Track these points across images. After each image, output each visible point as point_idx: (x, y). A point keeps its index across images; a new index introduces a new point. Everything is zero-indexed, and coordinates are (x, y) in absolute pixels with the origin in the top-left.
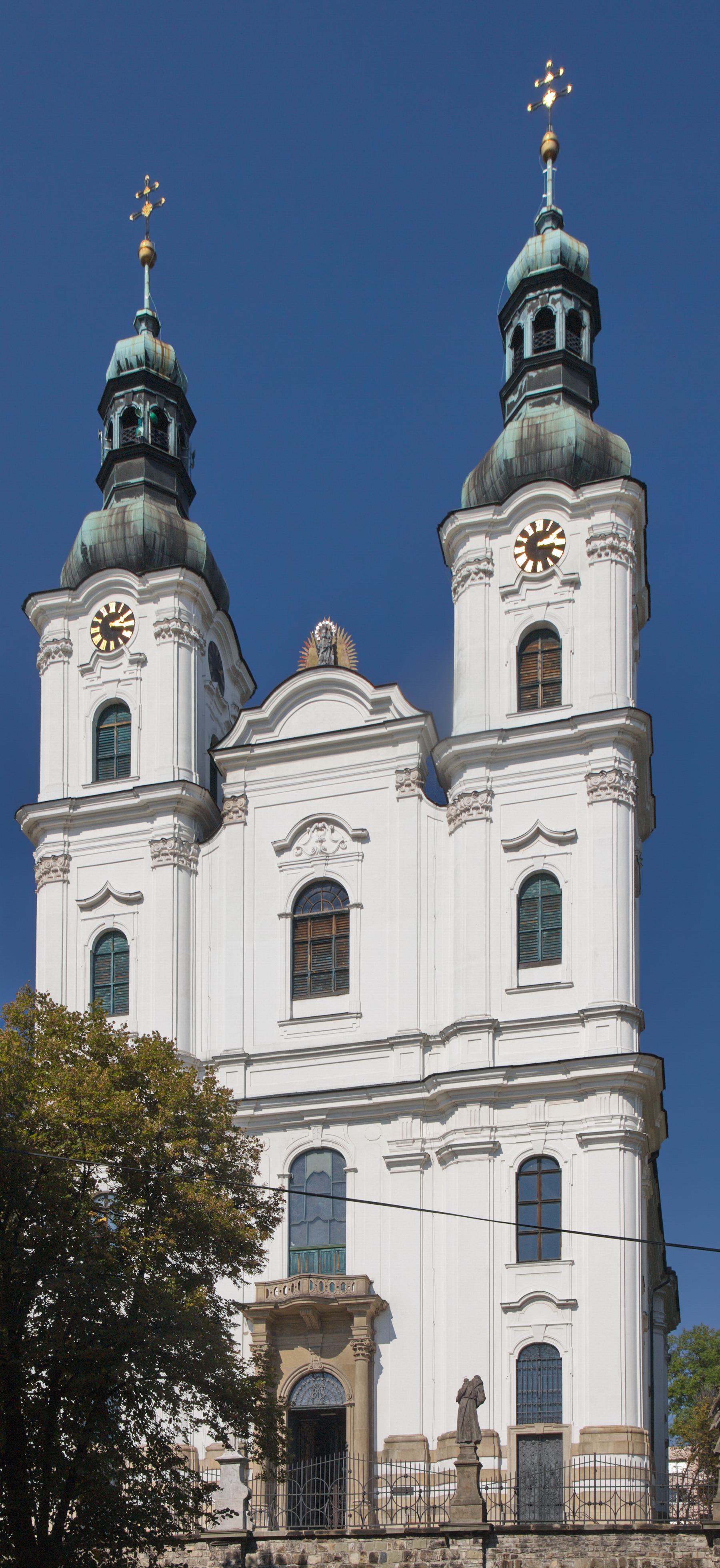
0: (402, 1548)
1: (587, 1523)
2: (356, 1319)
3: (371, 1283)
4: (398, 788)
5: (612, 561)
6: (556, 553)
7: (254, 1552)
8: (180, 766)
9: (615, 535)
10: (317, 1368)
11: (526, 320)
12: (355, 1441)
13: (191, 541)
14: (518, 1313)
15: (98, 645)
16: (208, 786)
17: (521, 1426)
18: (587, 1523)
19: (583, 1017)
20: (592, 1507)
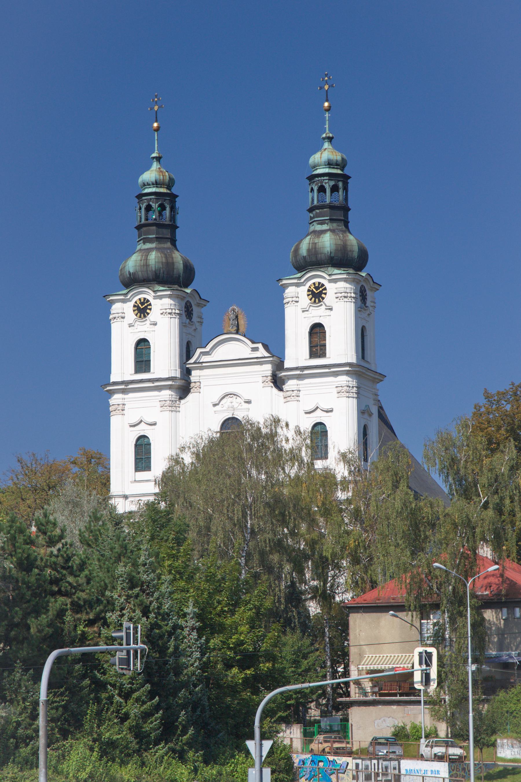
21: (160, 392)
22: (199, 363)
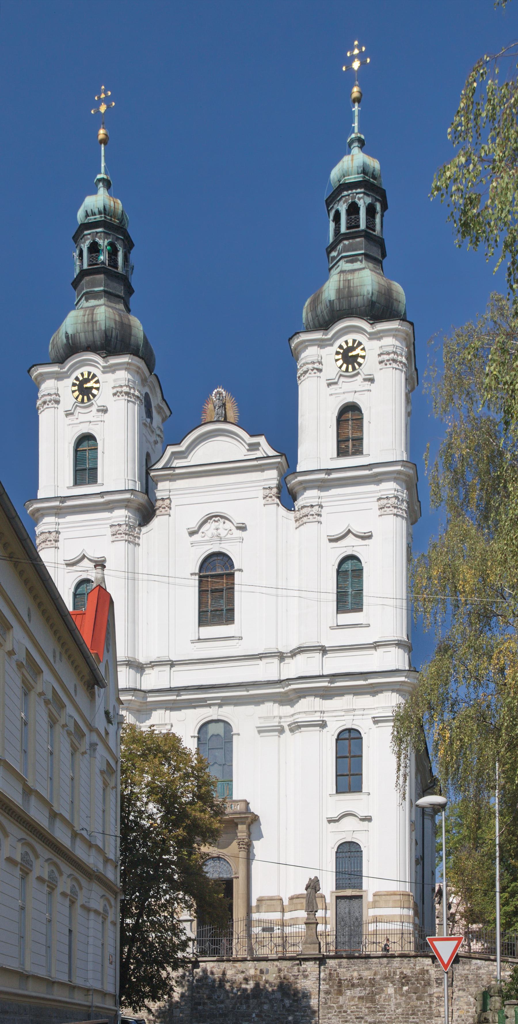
0: (277, 966)
1: (372, 953)
2: (239, 826)
3: (248, 804)
4: (264, 498)
5: (393, 368)
7: (198, 968)
9: (395, 353)
11: (343, 208)
12: (239, 900)
13: (134, 331)
14: (337, 823)
15: (77, 398)
16: (144, 491)
17: (338, 891)
18: (372, 953)
19: (376, 646)
20: (375, 944)
21: (111, 513)
22: (171, 468)
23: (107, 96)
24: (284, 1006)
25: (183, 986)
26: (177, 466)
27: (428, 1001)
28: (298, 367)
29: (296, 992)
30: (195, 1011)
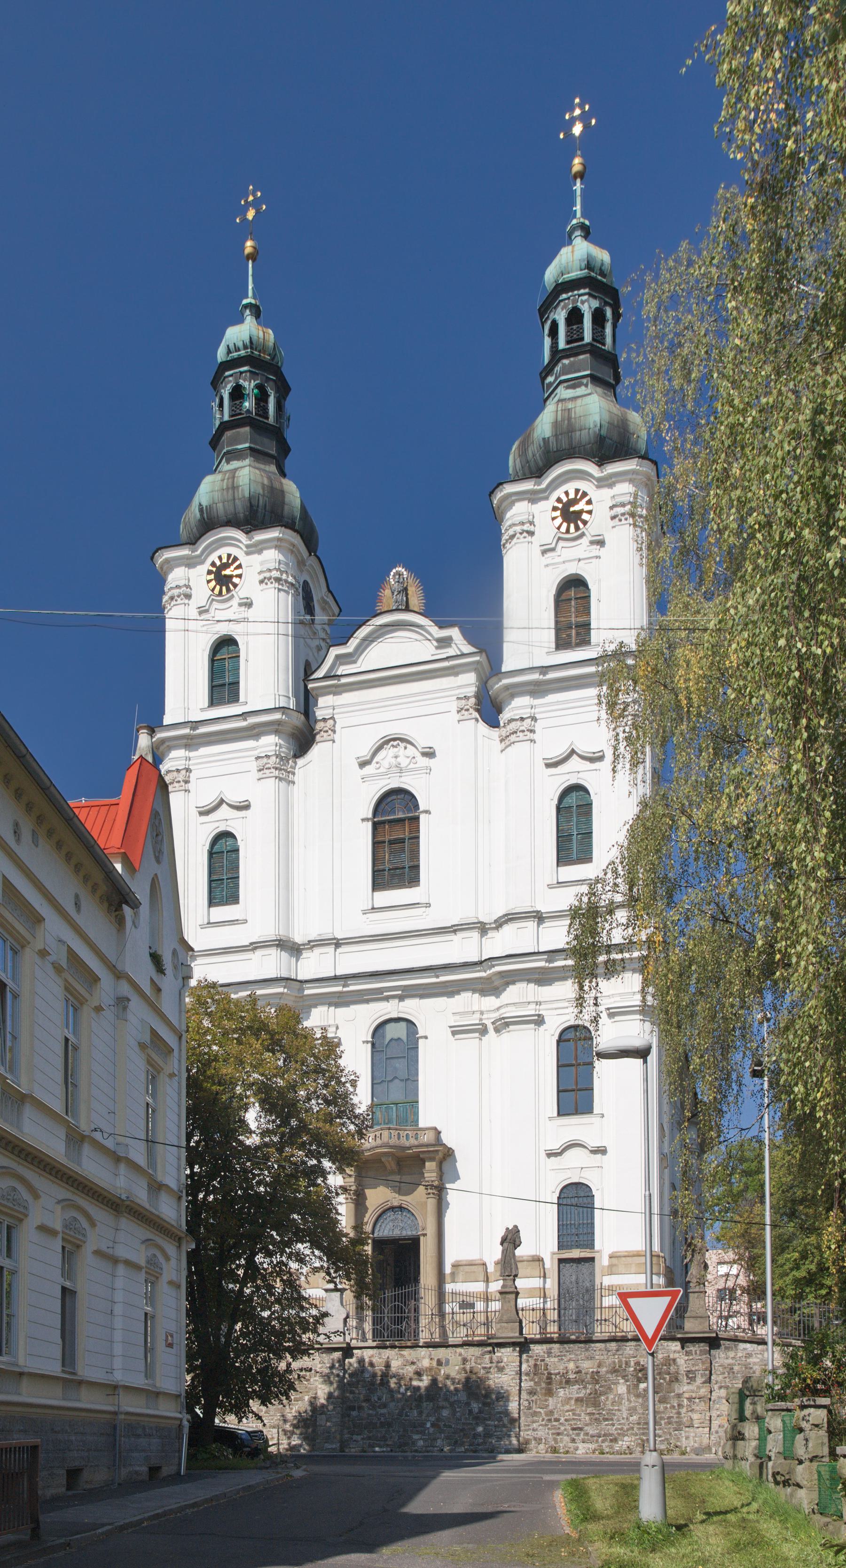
0: (460, 1355)
2: (427, 1164)
3: (439, 1133)
4: (458, 712)
6: (585, 516)
8: (281, 693)
10: (396, 1204)
11: (560, 316)
13: (288, 498)
15: (213, 590)
16: (302, 710)
21: (257, 741)
23: (255, 199)
24: (471, 1412)
25: (331, 1383)
26: (344, 673)
27: (676, 1404)
28: (503, 531)
29: (489, 1391)
30: (347, 1419)
